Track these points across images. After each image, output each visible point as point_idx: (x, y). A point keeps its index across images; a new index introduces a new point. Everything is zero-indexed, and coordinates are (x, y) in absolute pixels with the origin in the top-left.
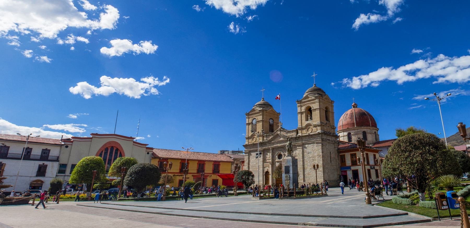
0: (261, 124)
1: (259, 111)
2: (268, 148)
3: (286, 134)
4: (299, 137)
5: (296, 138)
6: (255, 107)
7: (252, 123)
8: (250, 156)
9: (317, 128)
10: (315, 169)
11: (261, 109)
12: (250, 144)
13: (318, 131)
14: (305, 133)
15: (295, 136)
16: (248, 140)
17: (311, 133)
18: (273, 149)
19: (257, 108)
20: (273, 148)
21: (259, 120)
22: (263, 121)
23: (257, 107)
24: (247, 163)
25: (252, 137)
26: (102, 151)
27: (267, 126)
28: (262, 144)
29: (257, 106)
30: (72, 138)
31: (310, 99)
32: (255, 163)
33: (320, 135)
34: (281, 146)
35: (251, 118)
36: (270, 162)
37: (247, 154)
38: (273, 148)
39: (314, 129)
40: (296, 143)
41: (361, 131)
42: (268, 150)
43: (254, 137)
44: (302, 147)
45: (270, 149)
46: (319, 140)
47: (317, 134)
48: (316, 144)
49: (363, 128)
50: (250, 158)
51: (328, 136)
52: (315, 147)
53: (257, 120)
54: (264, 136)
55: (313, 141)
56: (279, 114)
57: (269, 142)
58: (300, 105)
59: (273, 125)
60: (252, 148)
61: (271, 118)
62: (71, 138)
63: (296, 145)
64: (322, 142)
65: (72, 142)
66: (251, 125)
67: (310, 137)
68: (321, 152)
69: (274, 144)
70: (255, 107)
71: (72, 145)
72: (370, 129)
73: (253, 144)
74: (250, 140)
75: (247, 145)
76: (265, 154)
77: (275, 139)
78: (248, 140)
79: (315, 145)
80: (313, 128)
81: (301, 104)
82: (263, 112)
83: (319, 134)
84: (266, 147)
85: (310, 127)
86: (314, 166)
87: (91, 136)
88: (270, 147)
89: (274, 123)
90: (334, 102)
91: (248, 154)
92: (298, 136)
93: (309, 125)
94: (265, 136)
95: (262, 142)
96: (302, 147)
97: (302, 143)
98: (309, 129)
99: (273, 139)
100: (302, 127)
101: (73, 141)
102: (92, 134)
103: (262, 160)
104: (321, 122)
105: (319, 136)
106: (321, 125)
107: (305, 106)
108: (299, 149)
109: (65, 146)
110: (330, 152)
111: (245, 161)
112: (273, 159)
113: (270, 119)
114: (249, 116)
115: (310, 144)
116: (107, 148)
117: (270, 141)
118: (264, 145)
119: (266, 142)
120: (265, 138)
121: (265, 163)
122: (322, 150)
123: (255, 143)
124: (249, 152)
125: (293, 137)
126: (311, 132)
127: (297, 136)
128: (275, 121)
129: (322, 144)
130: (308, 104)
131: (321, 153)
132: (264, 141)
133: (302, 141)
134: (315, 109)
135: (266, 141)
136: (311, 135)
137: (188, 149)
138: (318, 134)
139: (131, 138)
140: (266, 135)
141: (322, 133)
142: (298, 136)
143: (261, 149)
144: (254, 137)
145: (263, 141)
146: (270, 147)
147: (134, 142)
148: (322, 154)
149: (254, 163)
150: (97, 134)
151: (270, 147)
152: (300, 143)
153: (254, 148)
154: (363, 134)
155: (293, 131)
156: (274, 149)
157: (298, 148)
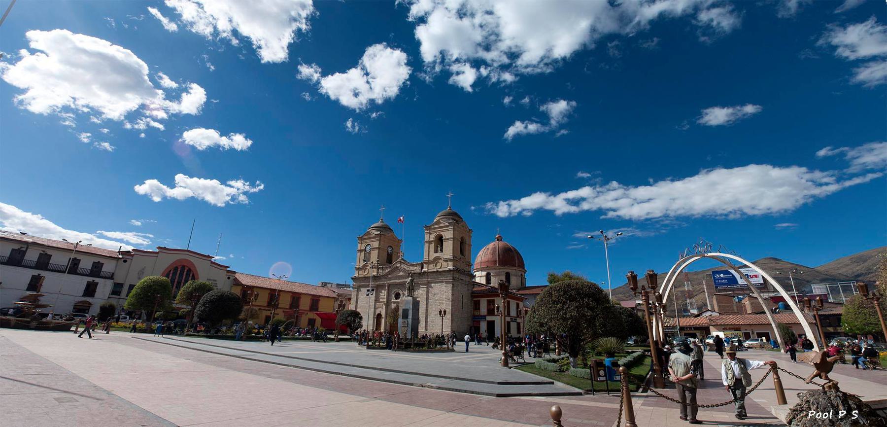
0: (376, 252)
4: (425, 272)
5: (420, 273)
7: (365, 250)
12: (360, 276)
13: (449, 268)
18: (389, 285)
25: (364, 268)
39: (445, 264)
46: (449, 278)
50: (359, 295)
57: (385, 276)
60: (363, 282)
65: (133, 256)
69: (390, 279)
74: (361, 272)
79: (444, 284)
83: (450, 271)
84: (381, 283)
87: (158, 251)
88: (387, 282)
92: (422, 271)
94: (381, 268)
99: (389, 273)
102: (159, 248)
109: (123, 260)
110: (463, 296)
115: (437, 283)
117: (386, 275)
123: (366, 276)
126: (440, 268)
129: (453, 285)
135: (381, 274)
136: (440, 272)
139: (209, 256)
141: (453, 271)
142: (422, 271)
147: (212, 262)
150: (165, 248)
152: (425, 280)
153: (365, 282)
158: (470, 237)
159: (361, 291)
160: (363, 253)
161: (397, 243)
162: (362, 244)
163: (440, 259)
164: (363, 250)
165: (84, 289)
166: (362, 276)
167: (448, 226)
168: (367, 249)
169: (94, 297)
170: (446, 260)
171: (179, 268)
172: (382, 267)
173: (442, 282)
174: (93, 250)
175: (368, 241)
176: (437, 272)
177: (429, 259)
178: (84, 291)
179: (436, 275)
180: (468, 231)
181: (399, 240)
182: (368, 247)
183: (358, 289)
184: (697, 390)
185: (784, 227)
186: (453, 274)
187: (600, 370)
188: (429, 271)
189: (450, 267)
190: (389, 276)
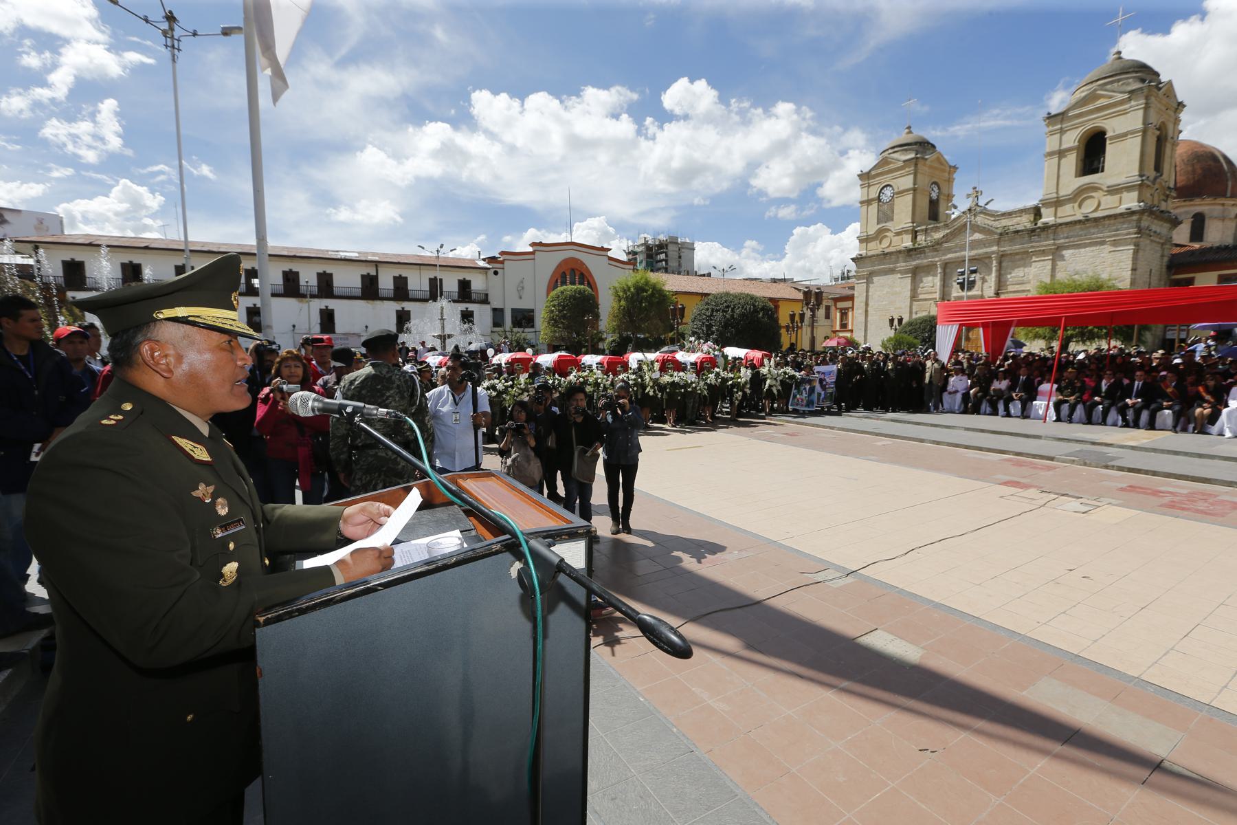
0: (909, 198)
1: (904, 161)
2: (931, 261)
3: (993, 222)
4: (1046, 227)
5: (1033, 231)
6: (891, 153)
7: (879, 199)
8: (870, 285)
9: (1121, 198)
10: (893, 327)
11: (912, 155)
12: (870, 253)
13: (904, 245)
14: (1070, 212)
15: (1029, 226)
16: (865, 244)
17: (887, 247)
18: (946, 265)
19: (895, 156)
20: (947, 261)
21: (901, 189)
22: (914, 190)
23: (894, 152)
24: (861, 302)
25: (880, 235)
26: (557, 280)
27: (924, 204)
28: (909, 253)
29: (896, 149)
30: (500, 254)
31: (1101, 102)
32: (886, 302)
33: (1135, 217)
34: (977, 257)
35: (878, 186)
36: (936, 299)
37: (863, 279)
38: (946, 264)
39: (896, 240)
40: (1032, 247)
41: (1187, 212)
42: (929, 269)
43: (886, 236)
44: (1051, 257)
45: (936, 265)
46: (1129, 232)
47: (1122, 215)
48: (1110, 247)
49: (1197, 201)
50: (870, 290)
51: (1156, 221)
52: (1102, 255)
53: (896, 190)
54: (916, 232)
55: (1101, 238)
56: (955, 168)
57: (936, 246)
58: (1059, 126)
59: (938, 200)
60: (879, 265)
61: (933, 181)
62: (498, 256)
63: (1107, 240)
64: (1137, 237)
65: (502, 262)
66: (877, 204)
67: (1088, 225)
68: (1130, 269)
69: (949, 250)
70: (891, 153)
71: (534, 259)
72: (1223, 205)
73: (881, 255)
74: (872, 245)
75: (865, 257)
76: (918, 278)
77: (954, 238)
78: (865, 244)
79: (1108, 248)
80: (892, 238)
81: (1061, 124)
82: (916, 165)
83: (1130, 213)
84: (925, 261)
85: (1093, 194)
86: (892, 321)
87: (530, 249)
88: (938, 259)
89: (942, 197)
90: (1184, 106)
91: (1053, 254)
92: (1039, 224)
93: (885, 229)
94: (922, 230)
95: (911, 247)
96: (865, 281)
97: (1054, 244)
98: (1088, 202)
99: (946, 238)
100: (1057, 197)
101: (504, 260)
102: (533, 244)
103: (909, 295)
104: (1141, 176)
105: (1130, 222)
106: (1140, 185)
107: (1083, 128)
108: (1042, 263)
109: (493, 270)
110: (1151, 270)
111: (858, 297)
112: (943, 292)
113: (932, 184)
114: (1064, 126)
115: (1085, 246)
116: (564, 272)
117: (939, 243)
118: (916, 255)
119: (925, 247)
120: (919, 238)
121: (915, 301)
122: (1133, 264)
123: (887, 251)
124: (870, 273)
125: (1020, 228)
126: (1096, 210)
127: (1036, 224)
128: (945, 190)
129: (1137, 245)
130: (1094, 121)
131: (1130, 272)
132: (917, 246)
133: (1054, 240)
134: (1124, 135)
135: (924, 244)
136: (1096, 220)
137: (723, 270)
138: (1127, 213)
139: (602, 249)
140: (924, 227)
141: (1141, 212)
142: (1039, 224)
143: (907, 266)
144: (886, 236)
145: (914, 245)
146: (937, 259)
147: (611, 259)
148: (1132, 274)
149: (884, 303)
150: (540, 244)
151: (937, 259)
152: (1048, 243)
153: (884, 264)
154: (1193, 222)
155: (1022, 211)
156: (949, 265)
157: (1034, 259)
158: (1177, 121)
159: (873, 283)
160: (875, 205)
161: (946, 175)
162: (869, 186)
163: (1096, 189)
164: (873, 200)
165: (395, 322)
166: (878, 252)
167: (1130, 99)
168: (883, 198)
169: (532, 311)
170: (1114, 190)
171: (568, 273)
172: (926, 230)
173: (1102, 243)
174: (452, 261)
175: (885, 180)
176: (1087, 220)
177: (1057, 193)
178: (397, 324)
179: (1082, 229)
180: (948, 169)
181: (950, 167)
182: (888, 192)
183: (869, 278)
184: (639, 437)
185: (97, 388)
186: (1139, 220)
187: (346, 413)
188: (1060, 221)
189: (1131, 201)
190: (946, 245)
